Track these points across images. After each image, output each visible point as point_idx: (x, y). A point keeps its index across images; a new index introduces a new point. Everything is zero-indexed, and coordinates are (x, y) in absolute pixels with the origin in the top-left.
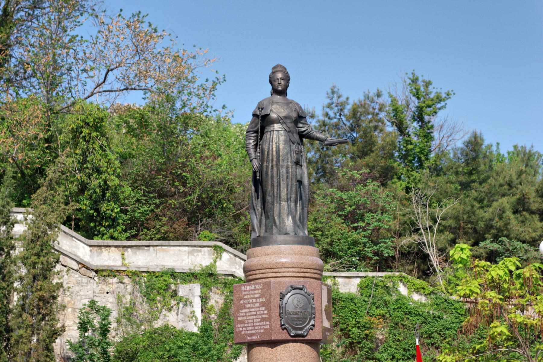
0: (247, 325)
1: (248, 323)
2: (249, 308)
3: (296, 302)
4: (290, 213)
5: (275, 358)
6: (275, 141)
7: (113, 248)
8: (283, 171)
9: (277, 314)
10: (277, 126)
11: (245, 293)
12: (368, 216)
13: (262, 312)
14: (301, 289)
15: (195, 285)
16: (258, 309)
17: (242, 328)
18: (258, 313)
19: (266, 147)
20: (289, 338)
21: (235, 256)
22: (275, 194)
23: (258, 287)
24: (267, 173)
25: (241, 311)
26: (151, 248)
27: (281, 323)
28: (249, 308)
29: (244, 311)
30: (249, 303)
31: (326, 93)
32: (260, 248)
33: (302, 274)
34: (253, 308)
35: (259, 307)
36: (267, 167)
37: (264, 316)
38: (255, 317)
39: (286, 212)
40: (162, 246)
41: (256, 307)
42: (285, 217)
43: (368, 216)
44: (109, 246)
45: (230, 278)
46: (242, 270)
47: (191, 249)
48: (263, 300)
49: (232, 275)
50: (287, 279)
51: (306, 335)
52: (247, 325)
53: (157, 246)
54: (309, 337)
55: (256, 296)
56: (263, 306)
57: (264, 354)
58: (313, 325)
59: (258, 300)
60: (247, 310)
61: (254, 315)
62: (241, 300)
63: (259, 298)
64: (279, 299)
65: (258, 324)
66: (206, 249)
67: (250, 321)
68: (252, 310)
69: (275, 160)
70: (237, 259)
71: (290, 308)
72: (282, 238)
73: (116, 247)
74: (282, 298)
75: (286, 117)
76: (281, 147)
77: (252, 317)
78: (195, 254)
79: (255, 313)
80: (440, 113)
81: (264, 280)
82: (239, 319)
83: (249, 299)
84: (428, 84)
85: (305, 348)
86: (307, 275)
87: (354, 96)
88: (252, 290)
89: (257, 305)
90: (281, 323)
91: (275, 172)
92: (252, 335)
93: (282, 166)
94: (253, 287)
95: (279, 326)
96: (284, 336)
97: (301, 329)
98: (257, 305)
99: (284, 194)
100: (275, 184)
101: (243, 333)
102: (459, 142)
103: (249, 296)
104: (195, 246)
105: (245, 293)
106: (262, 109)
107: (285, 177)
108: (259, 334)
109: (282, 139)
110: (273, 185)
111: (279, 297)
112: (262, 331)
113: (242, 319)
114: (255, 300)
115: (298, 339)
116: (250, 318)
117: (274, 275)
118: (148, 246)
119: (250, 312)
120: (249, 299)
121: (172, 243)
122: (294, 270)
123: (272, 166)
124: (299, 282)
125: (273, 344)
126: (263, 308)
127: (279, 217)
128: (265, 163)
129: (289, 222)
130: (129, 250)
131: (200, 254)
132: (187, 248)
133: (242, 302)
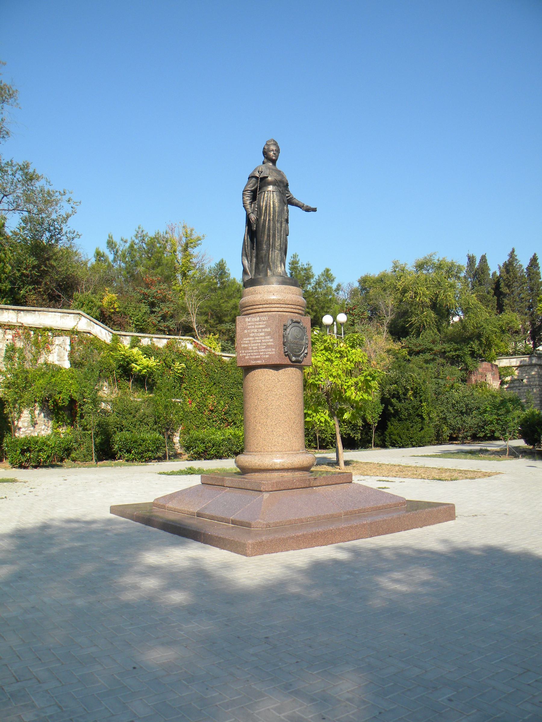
0: (251, 351)
1: (252, 349)
2: (253, 337)
5: (277, 380)
7: (11, 311)
9: (282, 343)
10: (271, 188)
11: (249, 324)
13: (267, 341)
15: (67, 337)
16: (263, 338)
17: (246, 353)
18: (263, 341)
19: (263, 204)
20: (290, 363)
21: (91, 320)
22: (271, 243)
23: (263, 318)
24: (264, 226)
25: (245, 339)
26: (37, 312)
27: (284, 350)
28: (253, 337)
29: (248, 339)
30: (253, 333)
31: (106, 238)
32: (263, 286)
34: (258, 337)
35: (265, 336)
36: (265, 221)
37: (269, 344)
38: (260, 344)
40: (43, 311)
41: (261, 336)
44: (9, 309)
45: (89, 335)
47: (62, 314)
48: (269, 330)
49: (89, 333)
52: (251, 351)
53: (40, 311)
55: (261, 326)
56: (268, 335)
57: (267, 376)
58: (307, 353)
59: (263, 330)
60: (251, 339)
61: (258, 343)
62: (245, 329)
64: (283, 330)
65: (263, 350)
66: (72, 315)
67: (255, 348)
68: (257, 338)
69: (272, 215)
70: (92, 323)
73: (13, 310)
77: (257, 345)
78: (65, 318)
79: (260, 341)
81: (269, 313)
82: (242, 346)
83: (253, 329)
84: (192, 230)
88: (256, 321)
89: (263, 334)
90: (284, 350)
92: (256, 359)
94: (258, 319)
95: (282, 353)
96: (287, 361)
98: (263, 334)
101: (247, 357)
102: (213, 265)
103: (253, 327)
104: (65, 313)
105: (249, 324)
106: (262, 172)
108: (264, 359)
110: (269, 236)
111: (282, 328)
112: (267, 356)
113: (246, 346)
114: (260, 330)
116: (254, 345)
117: (276, 309)
118: (35, 311)
119: (254, 340)
120: (253, 329)
121: (50, 309)
122: (292, 306)
123: (269, 220)
124: (297, 317)
125: (277, 367)
126: (269, 337)
128: (263, 216)
130: (22, 312)
131: (68, 318)
132: (60, 314)
133: (246, 331)
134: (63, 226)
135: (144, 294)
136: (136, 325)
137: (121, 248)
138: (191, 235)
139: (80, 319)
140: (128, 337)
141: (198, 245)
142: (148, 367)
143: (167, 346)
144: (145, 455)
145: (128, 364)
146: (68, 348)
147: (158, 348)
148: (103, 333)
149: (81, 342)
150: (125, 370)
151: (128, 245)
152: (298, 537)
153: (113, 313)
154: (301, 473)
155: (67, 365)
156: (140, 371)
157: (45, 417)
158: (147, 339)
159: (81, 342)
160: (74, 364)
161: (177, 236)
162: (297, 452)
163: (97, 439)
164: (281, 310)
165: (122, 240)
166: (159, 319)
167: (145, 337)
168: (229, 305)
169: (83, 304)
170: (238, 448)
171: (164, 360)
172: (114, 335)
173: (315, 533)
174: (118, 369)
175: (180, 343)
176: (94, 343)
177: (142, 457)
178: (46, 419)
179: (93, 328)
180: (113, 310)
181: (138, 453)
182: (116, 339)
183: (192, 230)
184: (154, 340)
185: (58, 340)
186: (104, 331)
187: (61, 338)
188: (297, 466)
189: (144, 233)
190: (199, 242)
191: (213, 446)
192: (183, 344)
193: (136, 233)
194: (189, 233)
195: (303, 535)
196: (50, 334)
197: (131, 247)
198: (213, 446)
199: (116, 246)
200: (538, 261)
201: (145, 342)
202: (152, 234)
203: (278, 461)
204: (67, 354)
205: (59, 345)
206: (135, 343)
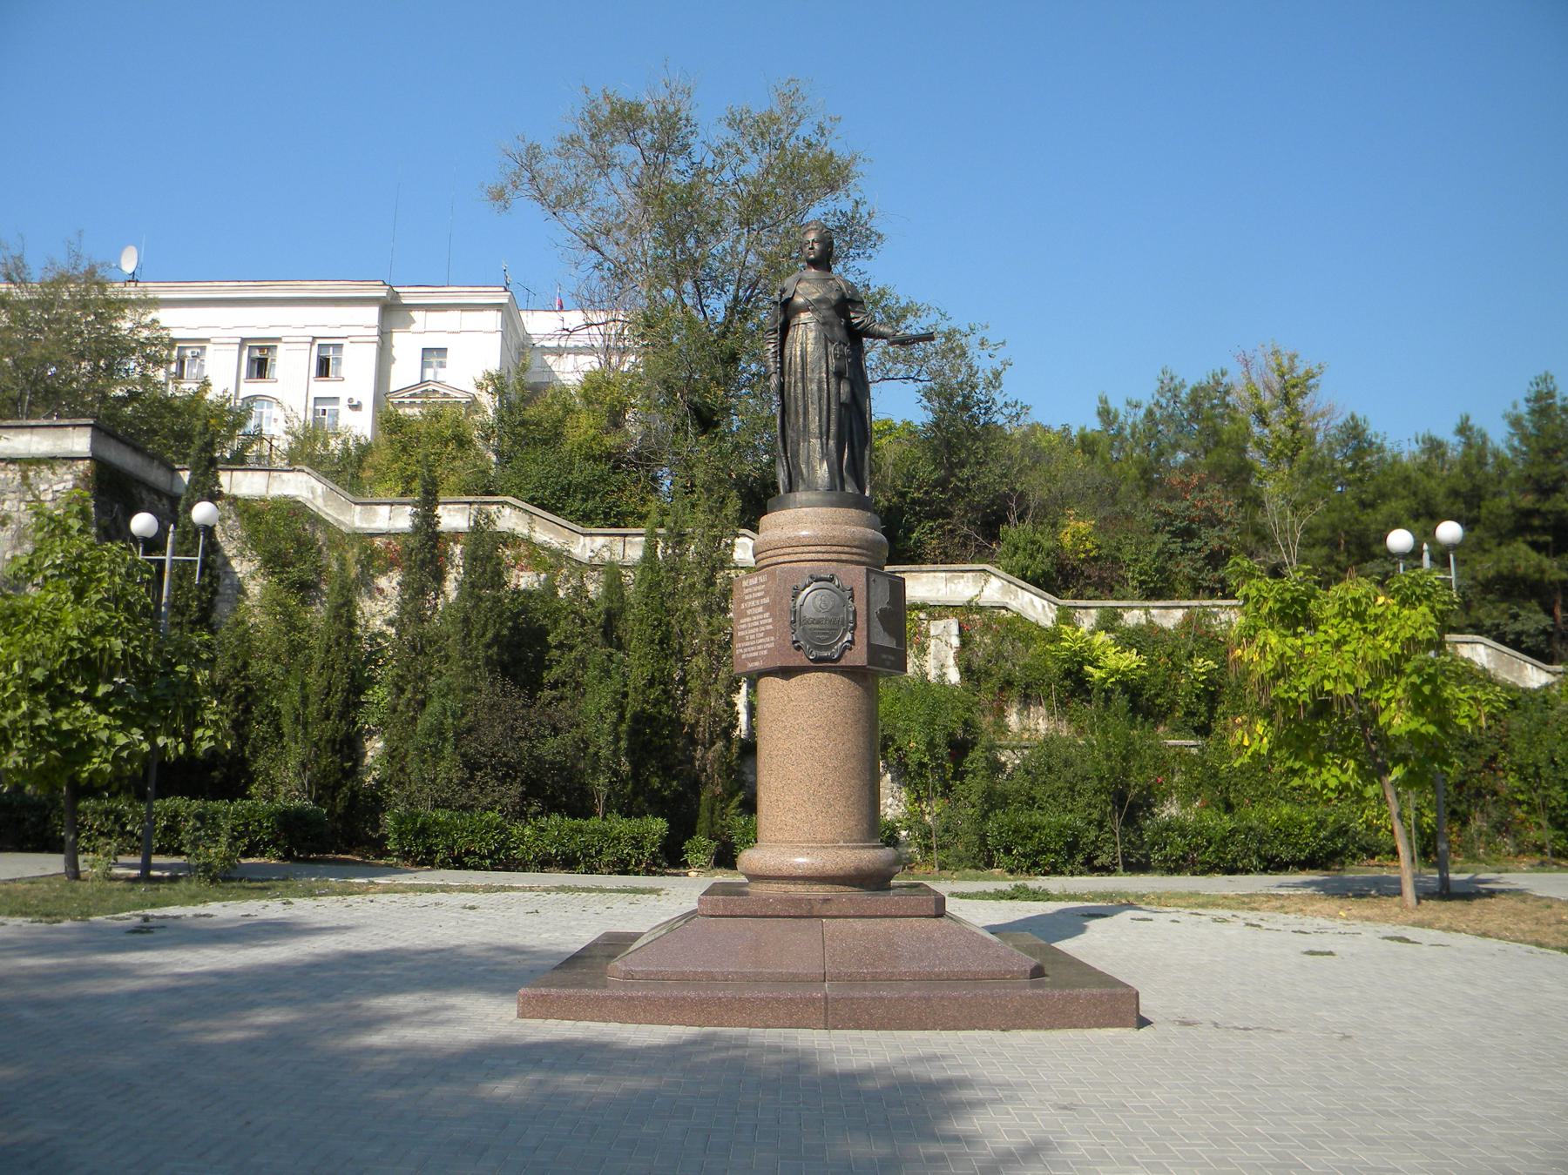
3: (818, 602)
4: (825, 455)
6: (799, 340)
8: (814, 387)
10: (804, 316)
12: (1205, 532)
14: (831, 580)
20: (808, 663)
33: (834, 556)
39: (818, 456)
42: (817, 464)
43: (1205, 532)
46: (750, 553)
48: (766, 600)
50: (808, 564)
51: (839, 659)
54: (842, 662)
71: (809, 613)
72: (812, 496)
74: (795, 597)
75: (818, 301)
76: (810, 348)
80: (1310, 395)
84: (1292, 358)
85: (838, 681)
86: (844, 557)
87: (1193, 376)
91: (799, 390)
92: (754, 659)
93: (811, 381)
95: (789, 644)
96: (799, 660)
97: (829, 648)
98: (760, 609)
99: (814, 426)
100: (801, 410)
107: (816, 397)
109: (811, 335)
115: (821, 664)
117: (787, 558)
124: (826, 569)
125: (786, 672)
127: (808, 463)
129: (822, 471)
134: (996, 394)
135: (1166, 514)
136: (1142, 583)
137: (1130, 421)
138: (1292, 370)
139: (986, 581)
140: (1093, 611)
141: (1310, 388)
142: (1117, 671)
143: (1188, 622)
144: (1042, 859)
145: (1081, 665)
146: (955, 642)
147: (1163, 630)
148: (1037, 607)
149: (987, 627)
150: (1073, 683)
151: (1142, 412)
152: (632, 998)
153: (1084, 561)
154: (828, 887)
155: (954, 676)
156: (1105, 680)
157: (893, 780)
158: (1136, 612)
159: (987, 627)
160: (967, 671)
161: (1265, 376)
162: (823, 844)
163: (1534, 835)
164: (795, 558)
165: (1129, 403)
166: (1200, 564)
167: (1132, 608)
168: (1379, 517)
169: (1017, 548)
170: (1301, 850)
171: (1169, 656)
172: (1060, 608)
173: (676, 999)
174: (1065, 678)
175: (1216, 615)
176: (1016, 629)
177: (1036, 864)
178: (895, 786)
179: (1016, 596)
180: (1083, 556)
181: (1024, 855)
182: (1065, 616)
183: (1292, 358)
184: (1153, 612)
185: (936, 628)
186: (1038, 601)
187: (941, 623)
188: (808, 873)
189: (1177, 381)
190: (1312, 382)
191: (1209, 843)
192: (1223, 617)
193: (1158, 384)
194: (1286, 363)
195: (646, 997)
196: (922, 616)
197: (1150, 413)
198: (1209, 843)
199: (1116, 417)
200: (898, 422)
201: (1133, 617)
202: (1191, 383)
203: (802, 861)
204: (951, 653)
205: (937, 637)
206: (1108, 622)
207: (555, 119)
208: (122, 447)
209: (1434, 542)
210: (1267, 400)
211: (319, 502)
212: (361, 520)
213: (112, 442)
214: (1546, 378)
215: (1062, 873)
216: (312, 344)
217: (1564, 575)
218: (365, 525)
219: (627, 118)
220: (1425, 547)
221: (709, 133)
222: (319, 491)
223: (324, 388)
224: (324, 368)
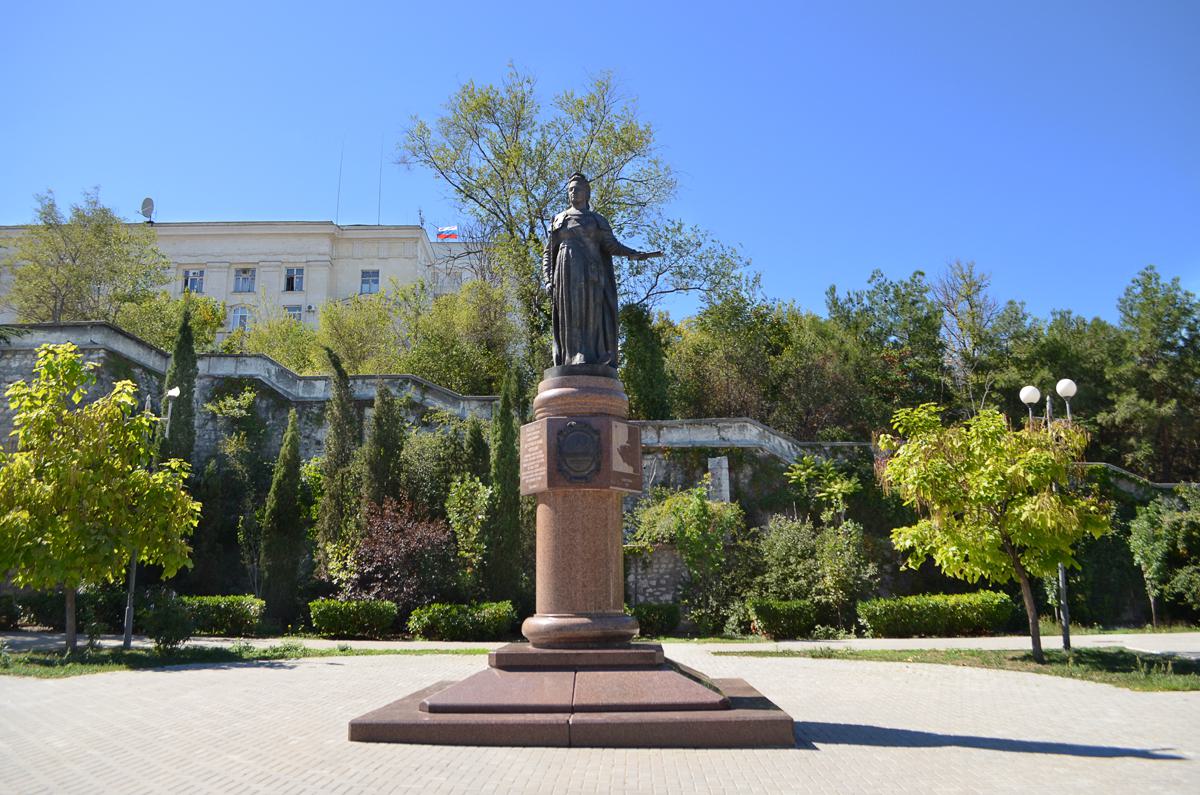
63: (539, 439)
92: (533, 483)
98: (537, 448)
112: (540, 478)
200: (1089, 320)
207: (434, 106)
208: (127, 340)
209: (1054, 395)
210: (408, 293)
211: (273, 379)
212: (303, 392)
213: (120, 337)
214: (1149, 277)
215: (1074, 677)
216: (229, 268)
217: (4, 363)
218: (306, 396)
219: (487, 109)
220: (1048, 398)
221: (545, 114)
222: (273, 372)
223: (293, 298)
224: (290, 286)
